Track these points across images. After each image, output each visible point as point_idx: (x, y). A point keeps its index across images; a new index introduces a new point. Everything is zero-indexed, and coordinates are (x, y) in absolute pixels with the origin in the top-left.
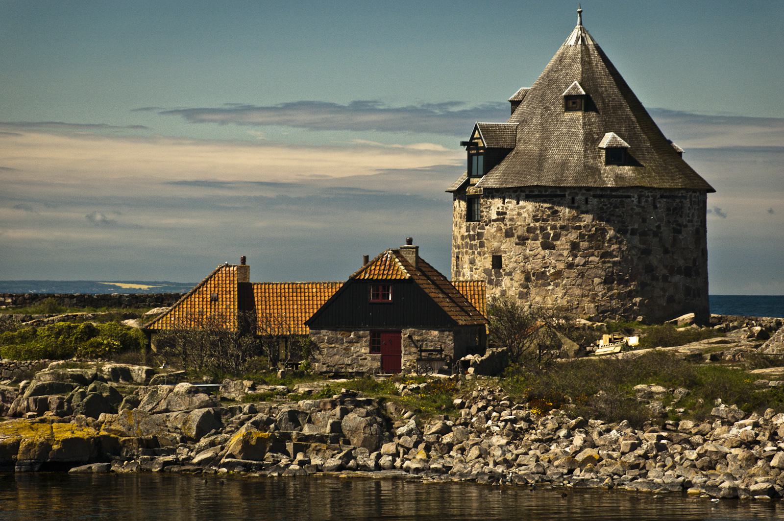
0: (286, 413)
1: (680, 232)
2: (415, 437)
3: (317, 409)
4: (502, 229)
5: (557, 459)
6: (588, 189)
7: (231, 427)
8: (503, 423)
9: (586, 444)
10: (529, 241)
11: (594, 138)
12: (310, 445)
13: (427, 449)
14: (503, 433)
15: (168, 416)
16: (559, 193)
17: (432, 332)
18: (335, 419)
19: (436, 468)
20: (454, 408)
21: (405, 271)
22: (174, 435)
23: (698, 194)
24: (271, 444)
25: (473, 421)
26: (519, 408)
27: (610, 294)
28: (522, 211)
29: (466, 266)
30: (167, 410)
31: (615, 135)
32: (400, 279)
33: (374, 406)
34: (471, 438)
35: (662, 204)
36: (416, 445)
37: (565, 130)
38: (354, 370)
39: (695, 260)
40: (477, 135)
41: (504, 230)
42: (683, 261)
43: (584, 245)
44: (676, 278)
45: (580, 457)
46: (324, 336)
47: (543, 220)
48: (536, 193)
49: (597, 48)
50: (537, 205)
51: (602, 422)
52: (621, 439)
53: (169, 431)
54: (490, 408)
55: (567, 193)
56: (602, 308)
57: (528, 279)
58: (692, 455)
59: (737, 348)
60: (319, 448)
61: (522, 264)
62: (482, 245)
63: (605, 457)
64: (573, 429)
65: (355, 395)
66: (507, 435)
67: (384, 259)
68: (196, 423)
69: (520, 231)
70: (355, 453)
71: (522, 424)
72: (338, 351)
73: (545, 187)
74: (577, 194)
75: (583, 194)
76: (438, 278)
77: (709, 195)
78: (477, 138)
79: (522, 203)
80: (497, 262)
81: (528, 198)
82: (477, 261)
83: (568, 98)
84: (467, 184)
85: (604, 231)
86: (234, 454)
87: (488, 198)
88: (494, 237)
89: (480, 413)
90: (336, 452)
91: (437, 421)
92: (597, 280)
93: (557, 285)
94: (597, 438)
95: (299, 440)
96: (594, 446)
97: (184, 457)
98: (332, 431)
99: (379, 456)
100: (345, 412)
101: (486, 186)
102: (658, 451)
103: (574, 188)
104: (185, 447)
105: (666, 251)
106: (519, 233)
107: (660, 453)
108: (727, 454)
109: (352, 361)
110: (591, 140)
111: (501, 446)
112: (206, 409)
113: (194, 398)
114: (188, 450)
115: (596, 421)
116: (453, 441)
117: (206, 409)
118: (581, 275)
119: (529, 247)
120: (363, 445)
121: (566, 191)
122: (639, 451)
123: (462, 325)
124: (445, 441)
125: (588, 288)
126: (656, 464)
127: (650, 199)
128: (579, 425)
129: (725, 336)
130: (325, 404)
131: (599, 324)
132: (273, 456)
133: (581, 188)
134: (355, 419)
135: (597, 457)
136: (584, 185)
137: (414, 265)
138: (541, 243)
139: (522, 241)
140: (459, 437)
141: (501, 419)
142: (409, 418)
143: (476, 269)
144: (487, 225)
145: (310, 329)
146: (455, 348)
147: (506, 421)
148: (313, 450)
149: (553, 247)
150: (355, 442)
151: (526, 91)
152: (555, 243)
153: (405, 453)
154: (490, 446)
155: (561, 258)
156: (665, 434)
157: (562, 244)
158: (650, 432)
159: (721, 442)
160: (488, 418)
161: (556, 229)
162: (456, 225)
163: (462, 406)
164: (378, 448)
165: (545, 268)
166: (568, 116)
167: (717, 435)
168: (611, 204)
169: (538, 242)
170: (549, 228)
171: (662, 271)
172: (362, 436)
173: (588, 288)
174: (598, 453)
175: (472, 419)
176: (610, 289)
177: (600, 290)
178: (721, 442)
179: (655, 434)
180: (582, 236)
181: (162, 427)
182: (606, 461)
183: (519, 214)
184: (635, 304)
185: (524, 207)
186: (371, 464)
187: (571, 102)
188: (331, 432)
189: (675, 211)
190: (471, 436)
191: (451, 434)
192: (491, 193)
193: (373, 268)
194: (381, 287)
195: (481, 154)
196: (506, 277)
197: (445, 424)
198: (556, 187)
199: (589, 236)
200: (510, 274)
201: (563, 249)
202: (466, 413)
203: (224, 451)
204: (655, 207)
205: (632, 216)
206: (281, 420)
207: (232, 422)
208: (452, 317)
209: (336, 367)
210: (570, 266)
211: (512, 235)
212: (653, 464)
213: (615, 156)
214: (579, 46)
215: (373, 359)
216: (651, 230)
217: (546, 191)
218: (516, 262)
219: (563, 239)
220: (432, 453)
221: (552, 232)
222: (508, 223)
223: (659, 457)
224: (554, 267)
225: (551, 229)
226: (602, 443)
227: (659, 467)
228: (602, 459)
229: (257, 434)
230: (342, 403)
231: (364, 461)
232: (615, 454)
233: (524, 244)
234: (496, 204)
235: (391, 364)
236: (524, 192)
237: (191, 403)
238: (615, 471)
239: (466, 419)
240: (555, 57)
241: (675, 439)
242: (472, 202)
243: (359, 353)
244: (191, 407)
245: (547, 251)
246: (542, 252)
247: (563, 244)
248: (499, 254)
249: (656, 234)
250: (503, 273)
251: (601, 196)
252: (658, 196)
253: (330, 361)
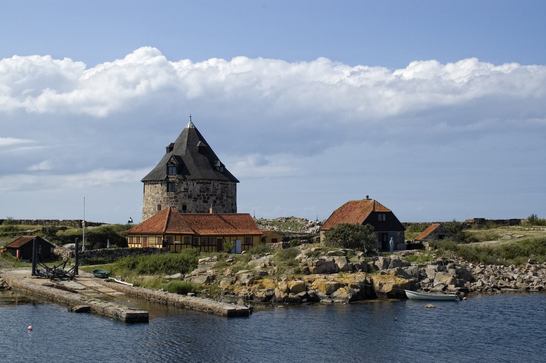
80: (184, 207)
139: (195, 200)
211: (194, 198)
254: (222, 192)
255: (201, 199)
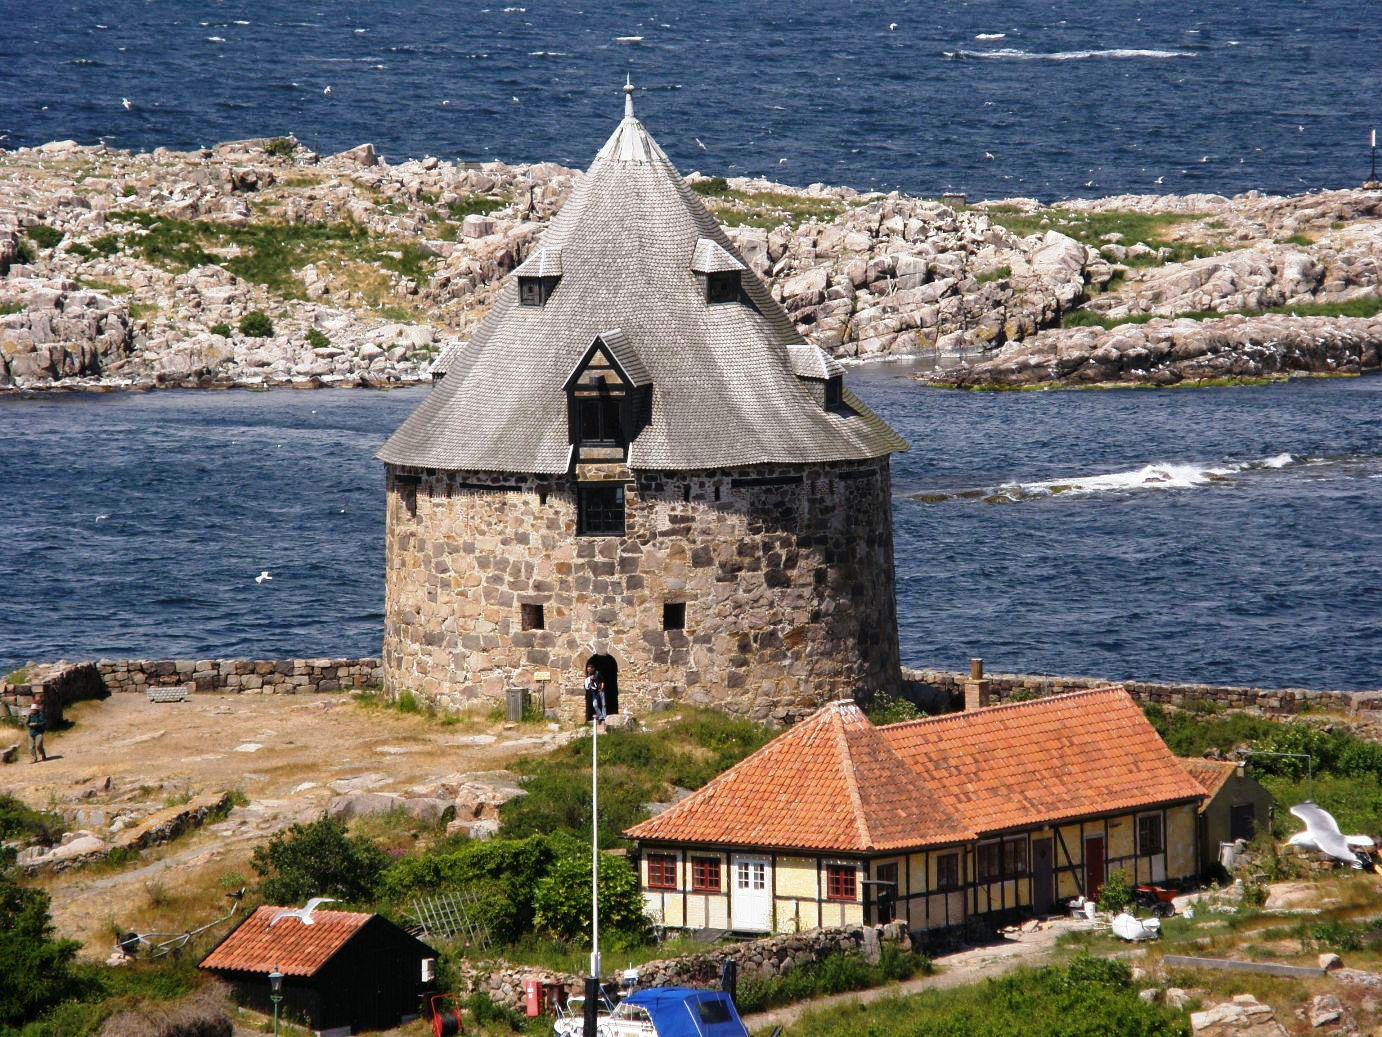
4: (683, 551)
10: (742, 573)
41: (689, 554)
57: (744, 647)
61: (731, 619)
62: (635, 583)
80: (673, 615)
93: (797, 656)
106: (723, 558)
119: (744, 585)
138: (766, 575)
139: (730, 572)
149: (786, 583)
152: (789, 573)
157: (801, 576)
158: (104, 65)
161: (790, 545)
165: (775, 624)
196: (697, 646)
200: (706, 639)
201: (804, 585)
210: (816, 616)
211: (709, 562)
217: (771, 472)
218: (719, 615)
221: (783, 553)
224: (791, 622)
225: (782, 546)
245: (777, 590)
246: (768, 593)
248: (679, 601)
250: (691, 638)
254: (848, 519)
255: (755, 568)
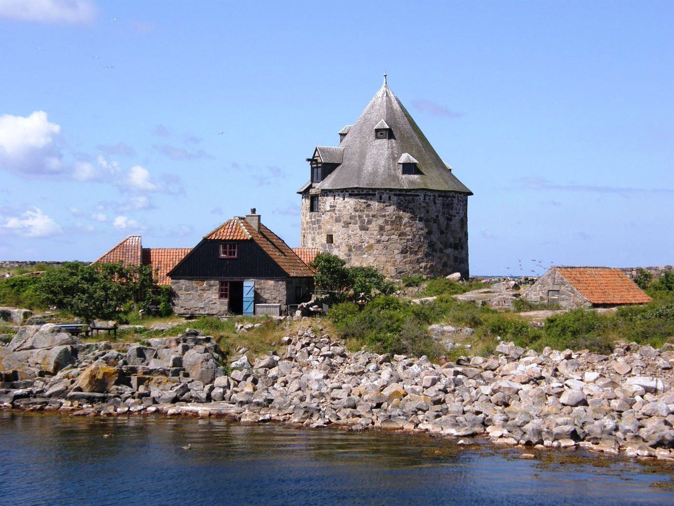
0: (135, 350)
1: (450, 220)
2: (245, 371)
3: (163, 346)
5: (366, 393)
6: (391, 190)
7: (86, 362)
8: (322, 358)
9: (392, 378)
11: (394, 157)
12: (152, 379)
13: (255, 382)
14: (321, 367)
15: (32, 353)
16: (371, 192)
17: (269, 281)
18: (177, 355)
19: (258, 402)
20: (282, 345)
21: (248, 233)
22: (33, 369)
23: (463, 195)
24: (117, 378)
25: (297, 355)
26: (336, 345)
27: (405, 260)
28: (346, 205)
29: (310, 242)
30: (32, 348)
31: (409, 155)
32: (243, 240)
33: (212, 343)
34: (293, 372)
35: (439, 201)
36: (246, 377)
37: (375, 152)
38: (206, 312)
39: (460, 239)
40: (317, 154)
42: (453, 240)
43: (388, 227)
44: (449, 251)
45: (386, 392)
46: (182, 284)
47: (361, 211)
48: (356, 193)
49: (397, 99)
50: (357, 200)
51: (405, 357)
52: (423, 374)
53: (29, 366)
54: (312, 345)
55: (377, 193)
56: (400, 270)
57: (350, 250)
58: (486, 390)
59: (500, 297)
60: (160, 381)
61: (346, 240)
62: (320, 228)
63: (409, 392)
64: (381, 363)
65: (196, 334)
66: (325, 369)
67: (231, 224)
68: (54, 359)
69: (346, 218)
70: (190, 385)
71: (339, 360)
72: (193, 297)
73: (362, 188)
74: (383, 193)
75: (387, 194)
76: (277, 241)
77: (469, 197)
78: (317, 157)
79: (346, 199)
81: (351, 195)
82: (316, 239)
83: (377, 131)
84: (310, 187)
85: (401, 218)
86: (82, 387)
87: (324, 196)
88: (328, 222)
89: (303, 349)
90: (175, 384)
91: (266, 356)
92: (396, 251)
94: (401, 371)
95: (145, 373)
96: (400, 380)
97: (38, 390)
98: (174, 365)
99: (212, 388)
100: (186, 349)
101: (323, 188)
102: (456, 385)
103: (381, 189)
104: (41, 380)
105: (442, 233)
107: (457, 388)
108: (518, 390)
109: (205, 304)
110: (394, 158)
111: (318, 381)
112: (64, 347)
113: (56, 337)
114: (43, 383)
115: (400, 356)
116: (278, 374)
117: (64, 347)
118: (386, 247)
120: (201, 379)
121: (375, 191)
122: (440, 386)
123: (293, 277)
124: (270, 375)
125: (390, 256)
126: (455, 399)
127: (432, 197)
128: (387, 360)
129: (489, 288)
130: (170, 342)
131: (398, 280)
132: (117, 389)
133: (386, 189)
134: (194, 356)
135: (402, 392)
136: (388, 187)
137: (257, 230)
139: (347, 224)
140: (283, 371)
141: (320, 354)
142: (243, 353)
143: (316, 244)
144: (323, 214)
145: (172, 279)
146: (287, 295)
147: (325, 356)
148: (155, 382)
150: (194, 374)
151: (350, 128)
152: (369, 226)
153: (235, 386)
154: (308, 380)
155: (372, 236)
156: (460, 369)
159: (510, 377)
160: (309, 354)
161: (369, 216)
162: (303, 215)
163: (289, 342)
164: (213, 380)
166: (379, 141)
167: (506, 370)
168: (406, 200)
169: (357, 225)
170: (364, 216)
171: (439, 245)
172: (200, 370)
173: (390, 256)
174: (403, 388)
175: (296, 354)
176: (405, 257)
177: (399, 257)
178: (510, 377)
179: (452, 370)
180: (386, 222)
181: (23, 363)
182: (411, 396)
183: (345, 207)
184: (421, 268)
185: (347, 202)
186: (203, 395)
187: (379, 133)
188: (174, 366)
189: (448, 206)
190: (295, 370)
191: (277, 368)
192: (325, 193)
193: (222, 230)
194: (228, 246)
195: (320, 167)
197: (272, 359)
198: (369, 189)
199: (391, 222)
200: (338, 247)
202: (291, 348)
203: (74, 384)
204: (435, 203)
205: (419, 208)
206: (130, 356)
207: (88, 358)
208: (285, 270)
209: (192, 310)
211: (340, 221)
212: (453, 399)
213: (409, 168)
214: (385, 98)
215: (222, 304)
216: (432, 218)
219: (374, 223)
220: (259, 385)
222: (337, 213)
223: (457, 392)
226: (406, 376)
227: (457, 401)
228: (407, 394)
229: (104, 368)
230: (185, 341)
231: (197, 394)
232: (418, 388)
233: (348, 227)
234: (329, 200)
235: (236, 306)
236: (348, 192)
237: (53, 341)
238: (419, 407)
239: (291, 354)
240: (369, 105)
241: (470, 375)
242: (314, 199)
243: (210, 299)
244: (53, 344)
246: (360, 232)
247: (374, 227)
249: (435, 221)
251: (399, 195)
252: (437, 196)
253: (187, 305)
